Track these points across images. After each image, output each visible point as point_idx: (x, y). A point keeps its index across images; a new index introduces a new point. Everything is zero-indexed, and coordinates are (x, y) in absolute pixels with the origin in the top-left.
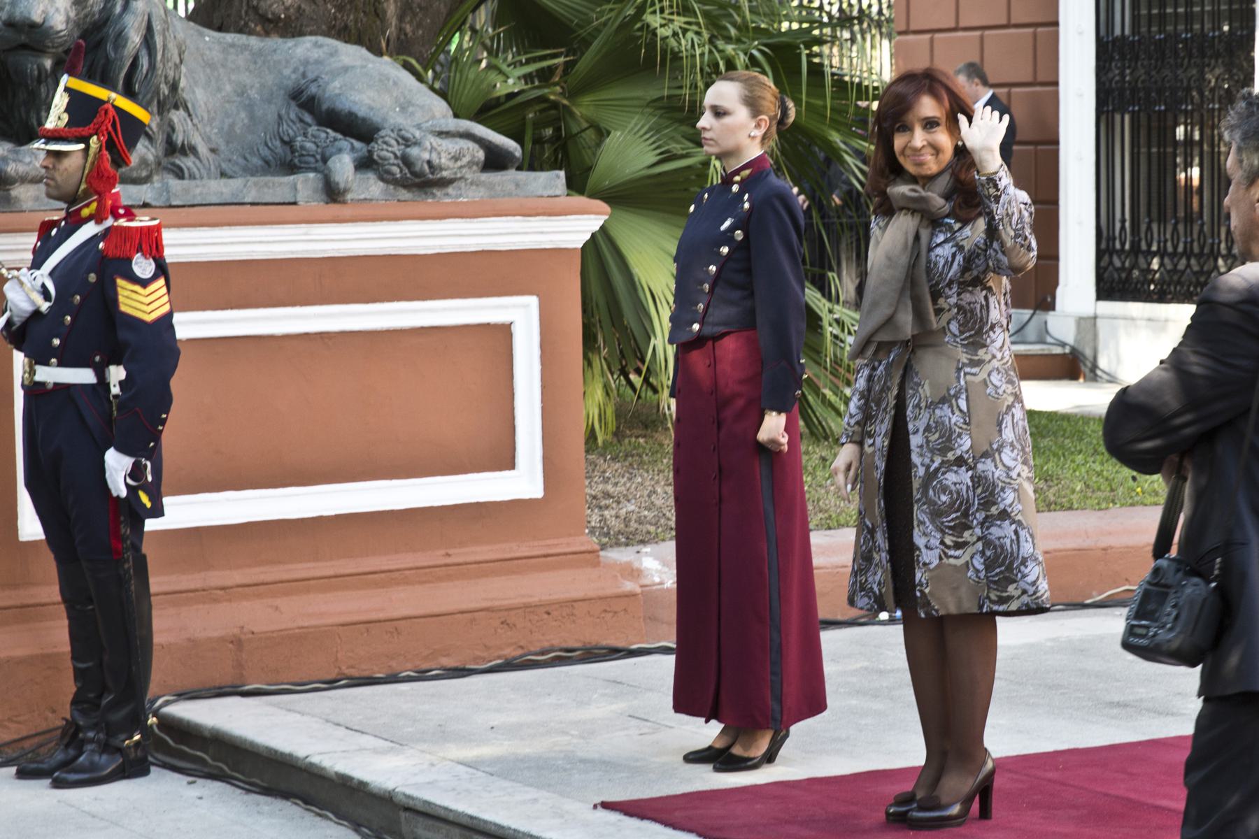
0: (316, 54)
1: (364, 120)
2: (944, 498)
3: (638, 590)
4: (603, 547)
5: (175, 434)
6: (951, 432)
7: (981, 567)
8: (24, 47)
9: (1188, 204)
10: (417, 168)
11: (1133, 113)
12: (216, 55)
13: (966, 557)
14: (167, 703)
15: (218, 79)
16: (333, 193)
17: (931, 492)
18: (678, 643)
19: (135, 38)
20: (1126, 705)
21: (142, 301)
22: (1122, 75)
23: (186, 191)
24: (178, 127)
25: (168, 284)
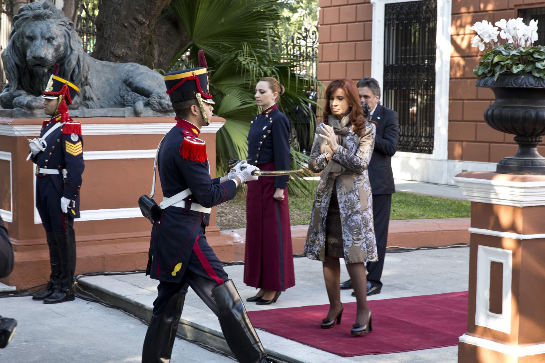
0: (132, 68)
1: (147, 90)
2: (353, 224)
3: (232, 244)
4: (221, 229)
5: (84, 191)
6: (354, 202)
7: (365, 247)
8: (38, 65)
9: (412, 119)
10: (164, 106)
11: (395, 90)
12: (99, 68)
13: (360, 244)
14: (81, 277)
15: (101, 76)
16: (137, 114)
17: (348, 222)
18: (245, 261)
19: (74, 63)
20: (391, 286)
21: (73, 149)
22: (392, 77)
23: (89, 112)
24: (87, 91)
25: (82, 144)
